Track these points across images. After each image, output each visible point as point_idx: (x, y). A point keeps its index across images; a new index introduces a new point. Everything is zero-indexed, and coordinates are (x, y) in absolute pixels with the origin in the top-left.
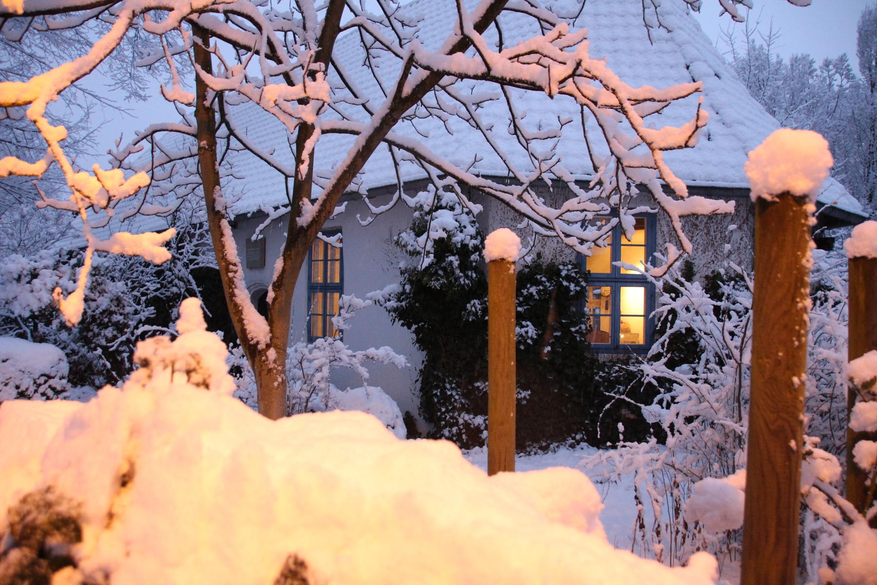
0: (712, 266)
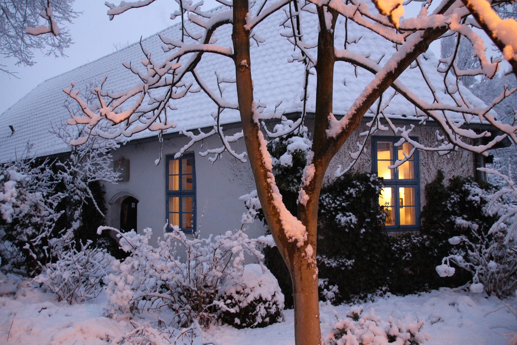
0: (453, 172)
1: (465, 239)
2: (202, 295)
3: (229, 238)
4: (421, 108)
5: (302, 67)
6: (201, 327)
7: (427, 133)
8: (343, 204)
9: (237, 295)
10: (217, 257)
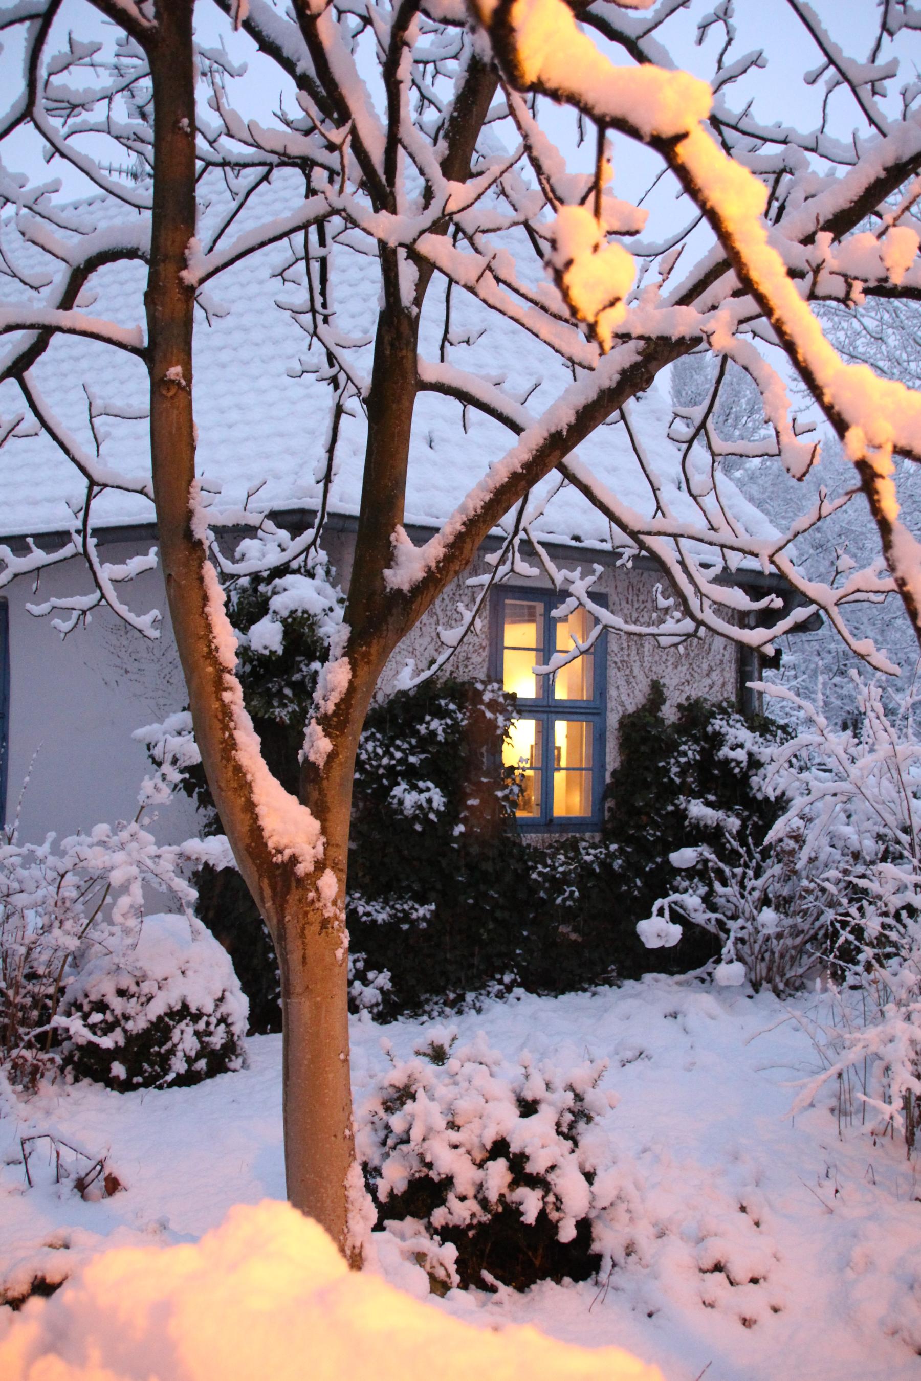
0: (687, 688)
1: (706, 851)
2: (19, 1000)
3: (102, 843)
4: (623, 527)
5: (325, 395)
6: (14, 1092)
7: (631, 585)
8: (412, 759)
9: (120, 999)
10: (67, 894)
